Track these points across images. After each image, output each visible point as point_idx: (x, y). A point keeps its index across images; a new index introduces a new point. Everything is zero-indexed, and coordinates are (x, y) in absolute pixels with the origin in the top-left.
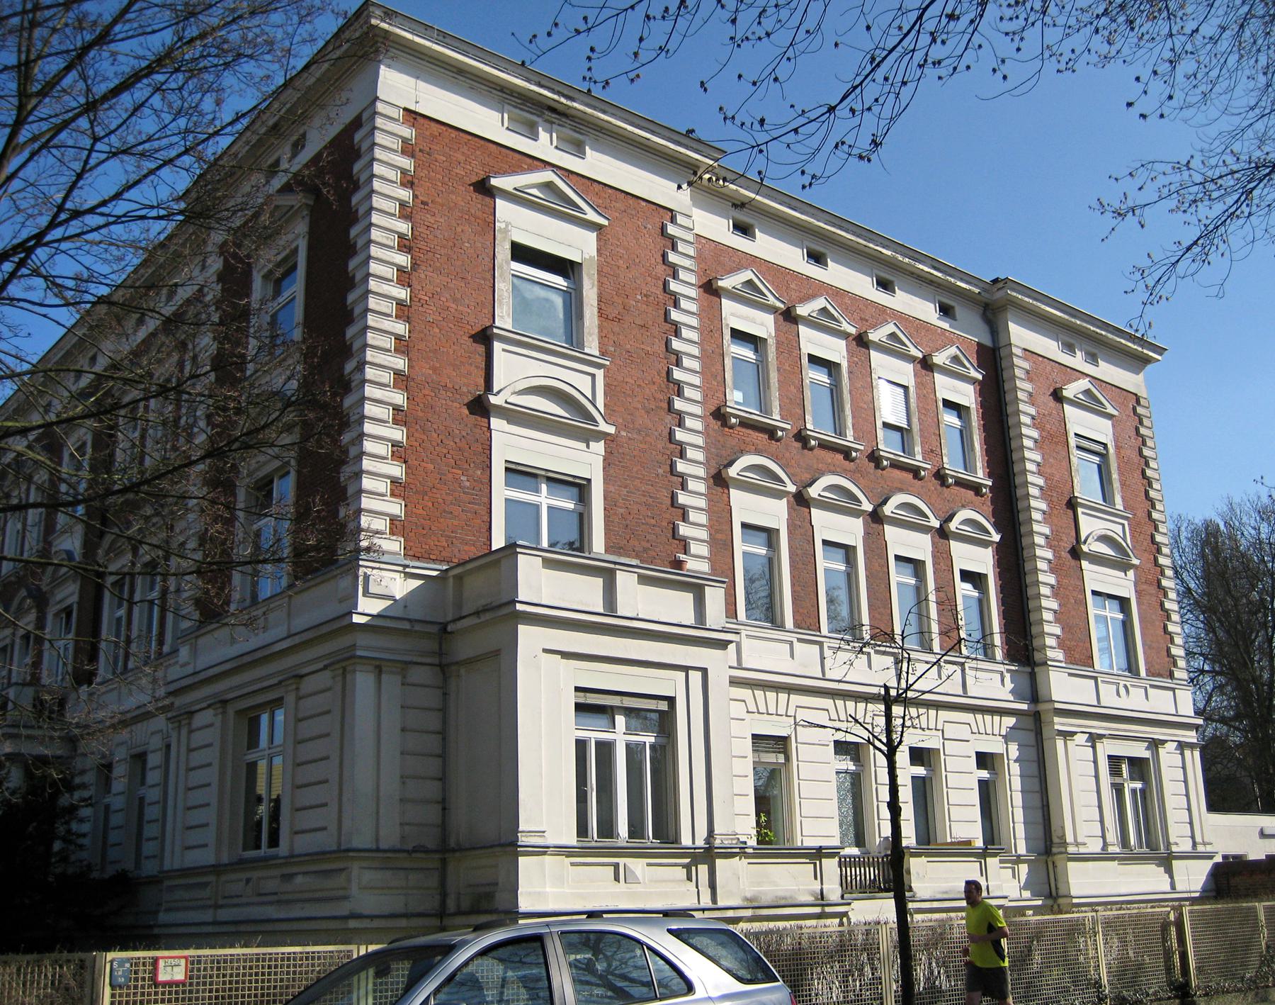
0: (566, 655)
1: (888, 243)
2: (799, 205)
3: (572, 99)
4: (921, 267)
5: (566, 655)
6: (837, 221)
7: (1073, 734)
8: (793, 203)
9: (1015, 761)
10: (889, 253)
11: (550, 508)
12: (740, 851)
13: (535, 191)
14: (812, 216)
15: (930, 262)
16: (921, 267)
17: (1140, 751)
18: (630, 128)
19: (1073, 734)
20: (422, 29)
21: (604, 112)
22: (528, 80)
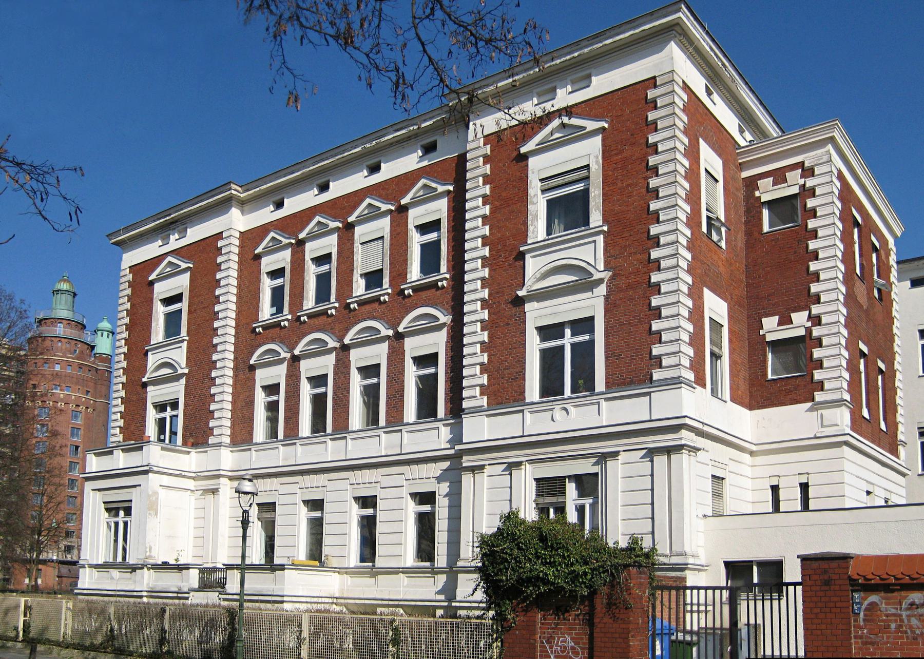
0: (99, 490)
1: (354, 143)
2: (293, 168)
3: (170, 215)
4: (386, 138)
5: (99, 490)
6: (318, 159)
7: (482, 467)
8: (289, 170)
9: (445, 496)
10: (359, 149)
11: (562, 348)
12: (295, 566)
13: (557, 135)
14: (305, 167)
15: (391, 129)
16: (386, 138)
17: (586, 467)
18: (211, 200)
19: (482, 467)
20: (649, 18)
21: (182, 209)
22: (155, 221)
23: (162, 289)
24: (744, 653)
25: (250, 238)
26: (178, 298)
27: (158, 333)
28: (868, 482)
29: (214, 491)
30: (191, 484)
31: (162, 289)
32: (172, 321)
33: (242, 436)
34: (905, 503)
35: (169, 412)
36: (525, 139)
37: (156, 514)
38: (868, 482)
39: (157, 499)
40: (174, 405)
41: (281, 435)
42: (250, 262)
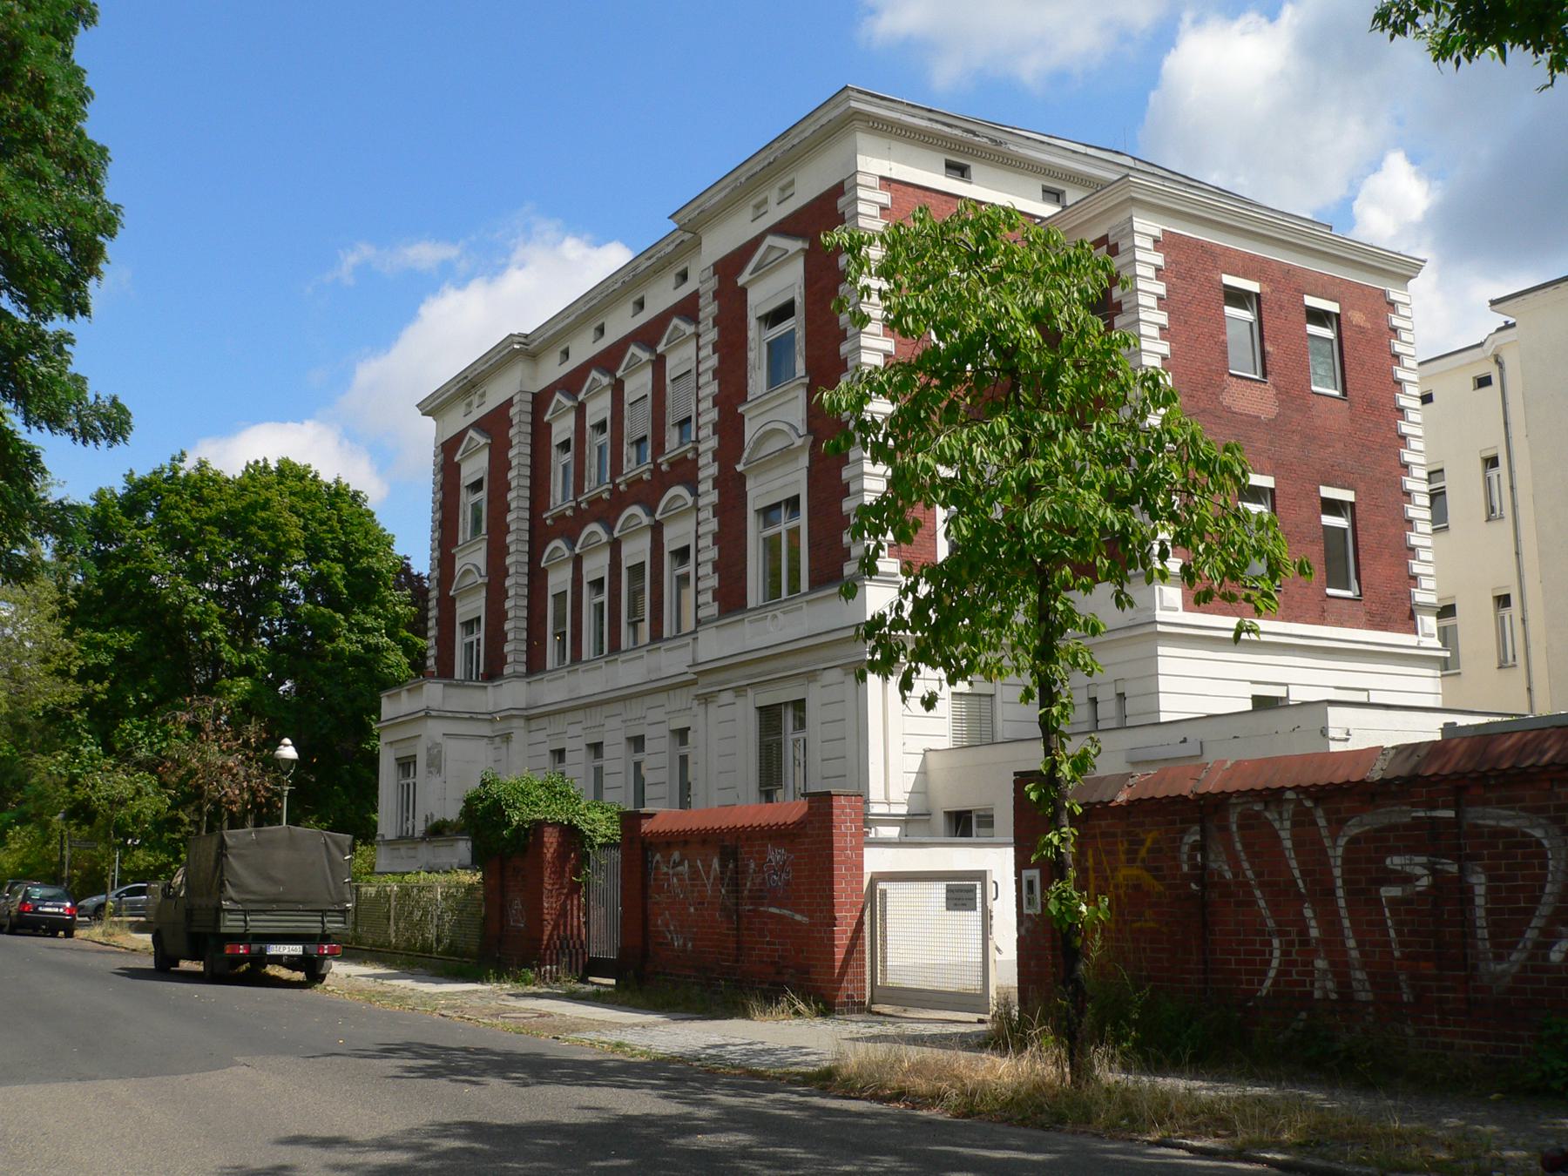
23: (761, 298)
24: (1564, 975)
25: (540, 401)
26: (785, 312)
27: (757, 380)
28: (1253, 682)
29: (507, 738)
30: (485, 729)
31: (761, 298)
32: (778, 352)
33: (535, 664)
34: (1439, 705)
35: (783, 526)
36: (739, 270)
37: (439, 772)
38: (1253, 682)
39: (440, 752)
40: (793, 503)
41: (606, 651)
42: (540, 432)
